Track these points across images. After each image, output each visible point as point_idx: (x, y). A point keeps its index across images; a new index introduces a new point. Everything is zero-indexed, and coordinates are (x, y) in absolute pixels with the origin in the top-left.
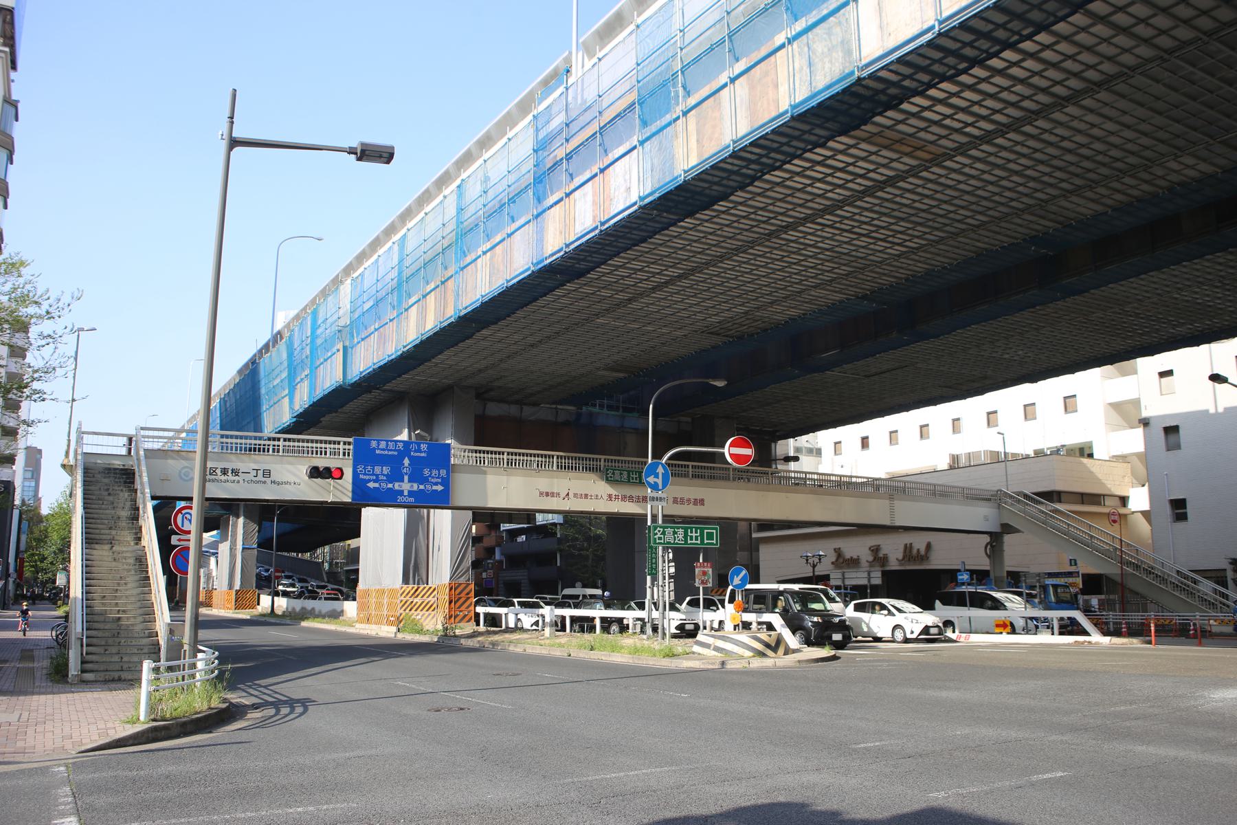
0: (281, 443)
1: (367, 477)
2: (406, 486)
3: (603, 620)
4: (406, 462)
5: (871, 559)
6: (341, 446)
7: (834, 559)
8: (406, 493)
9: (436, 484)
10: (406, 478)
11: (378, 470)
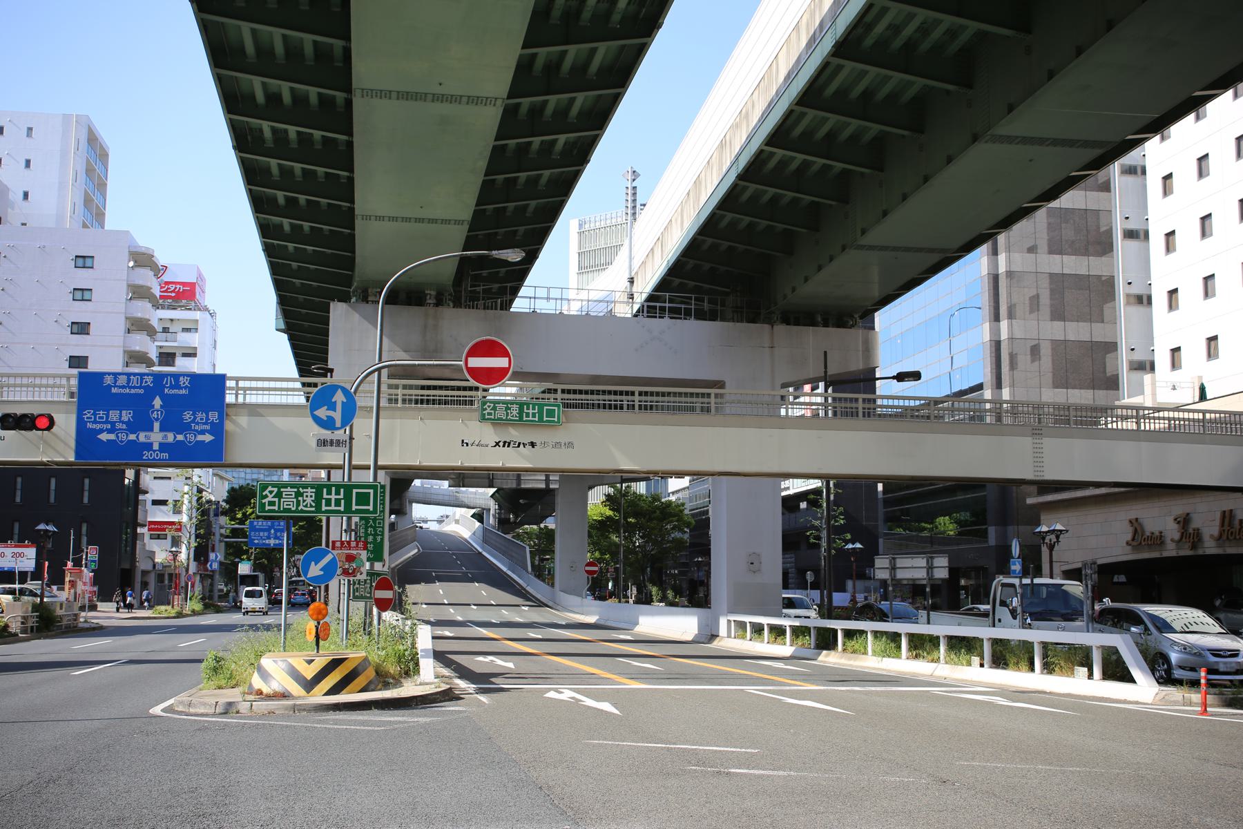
0: (400, 391)
1: (98, 426)
2: (156, 437)
3: (1045, 646)
4: (157, 402)
5: (1177, 536)
6: (637, 398)
7: (1129, 537)
8: (156, 447)
9: (203, 432)
10: (157, 425)
11: (114, 415)
